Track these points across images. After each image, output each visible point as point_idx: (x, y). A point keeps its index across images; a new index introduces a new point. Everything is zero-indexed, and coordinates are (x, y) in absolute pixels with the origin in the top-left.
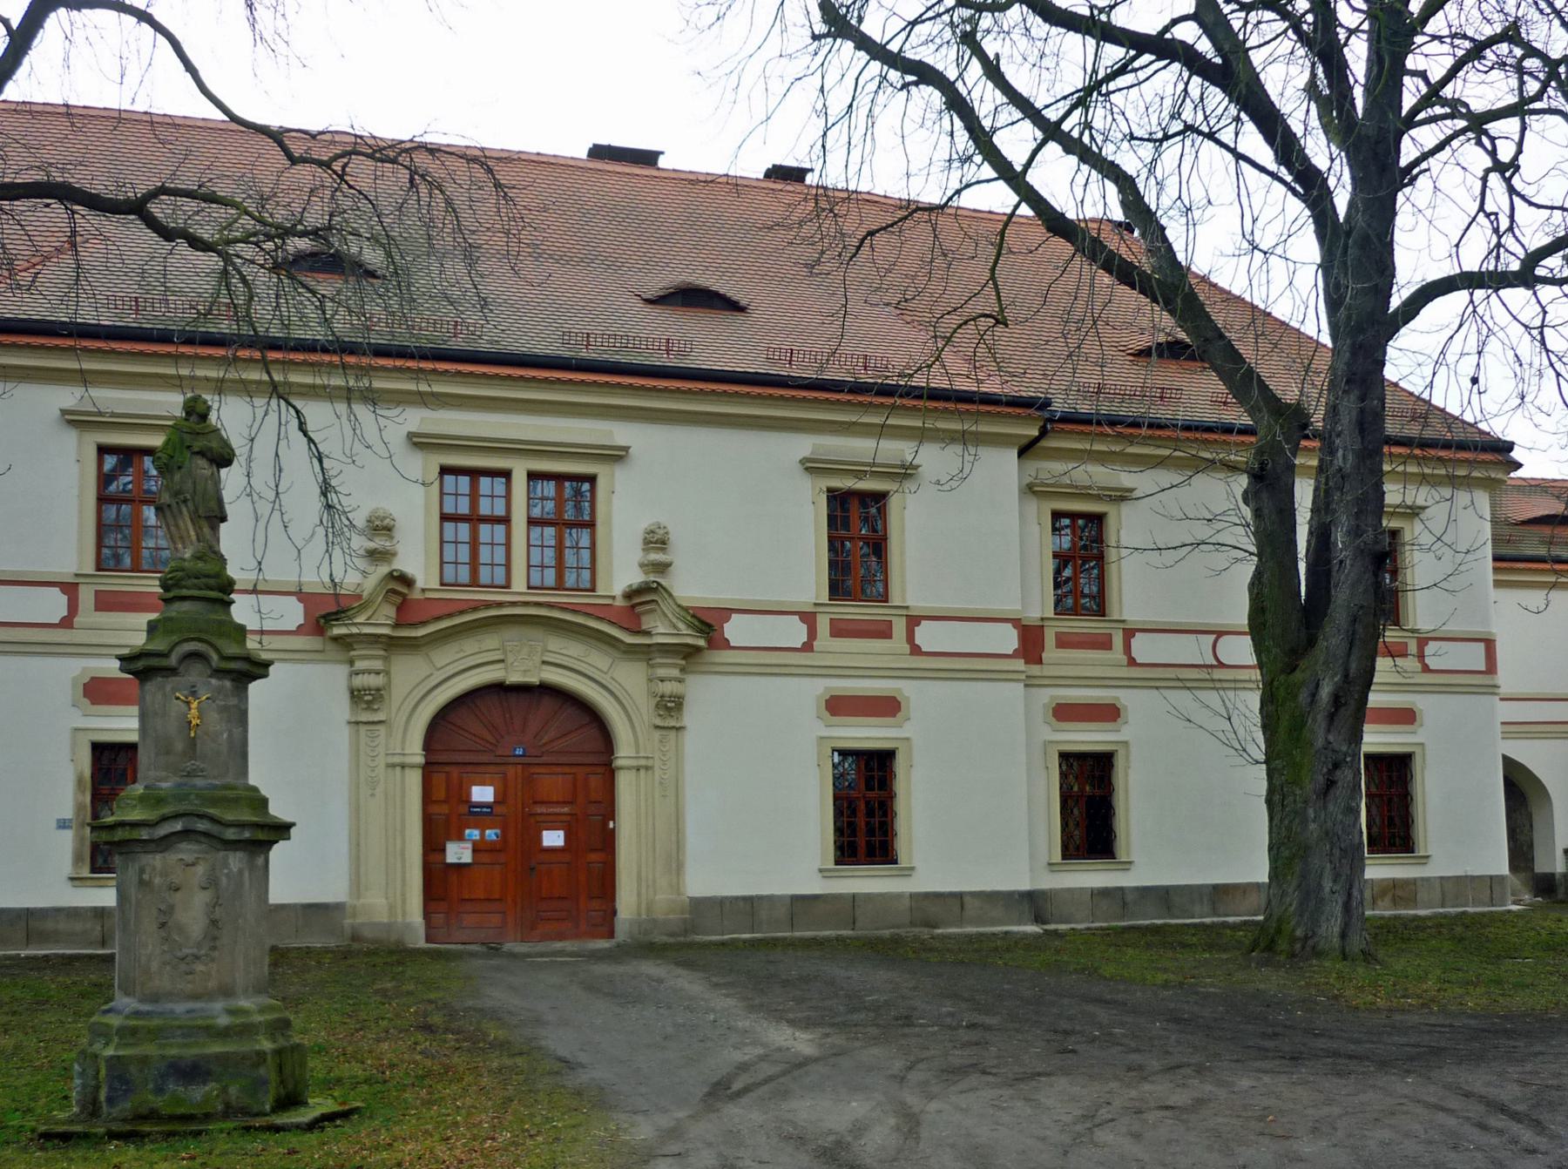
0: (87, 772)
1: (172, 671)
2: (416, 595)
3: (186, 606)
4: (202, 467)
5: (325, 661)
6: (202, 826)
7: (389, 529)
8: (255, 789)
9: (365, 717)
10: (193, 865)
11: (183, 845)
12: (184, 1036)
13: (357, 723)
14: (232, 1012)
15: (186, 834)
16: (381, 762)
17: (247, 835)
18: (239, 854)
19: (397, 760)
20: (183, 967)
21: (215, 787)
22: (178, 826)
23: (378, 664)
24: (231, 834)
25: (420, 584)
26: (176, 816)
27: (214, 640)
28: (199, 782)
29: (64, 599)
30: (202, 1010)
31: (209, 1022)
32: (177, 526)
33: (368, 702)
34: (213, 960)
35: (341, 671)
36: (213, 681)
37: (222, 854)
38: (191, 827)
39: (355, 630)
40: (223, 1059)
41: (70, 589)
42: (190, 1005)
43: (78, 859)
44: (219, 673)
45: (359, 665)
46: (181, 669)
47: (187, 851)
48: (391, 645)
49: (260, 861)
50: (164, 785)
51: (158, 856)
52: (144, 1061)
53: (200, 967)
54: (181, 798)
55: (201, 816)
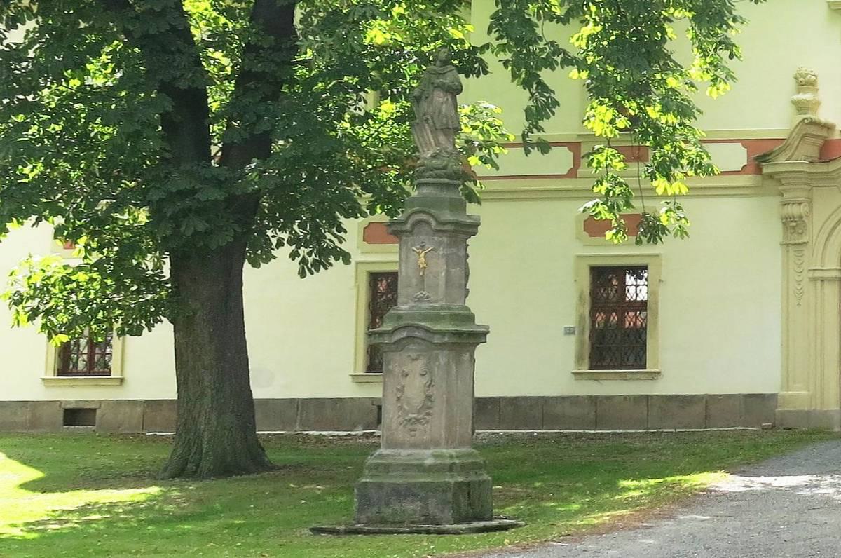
0: (587, 291)
3: (425, 190)
4: (439, 97)
6: (417, 334)
8: (468, 309)
11: (411, 346)
13: (788, 245)
14: (435, 456)
16: (806, 275)
17: (446, 339)
18: (446, 352)
19: (818, 274)
20: (409, 426)
21: (434, 308)
22: (405, 335)
23: (802, 196)
24: (437, 339)
26: (404, 327)
28: (424, 305)
30: (418, 454)
31: (420, 462)
32: (423, 136)
33: (794, 228)
35: (775, 201)
36: (436, 238)
40: (423, 486)
43: (579, 359)
48: (813, 181)
49: (466, 356)
53: (419, 426)
55: (418, 328)
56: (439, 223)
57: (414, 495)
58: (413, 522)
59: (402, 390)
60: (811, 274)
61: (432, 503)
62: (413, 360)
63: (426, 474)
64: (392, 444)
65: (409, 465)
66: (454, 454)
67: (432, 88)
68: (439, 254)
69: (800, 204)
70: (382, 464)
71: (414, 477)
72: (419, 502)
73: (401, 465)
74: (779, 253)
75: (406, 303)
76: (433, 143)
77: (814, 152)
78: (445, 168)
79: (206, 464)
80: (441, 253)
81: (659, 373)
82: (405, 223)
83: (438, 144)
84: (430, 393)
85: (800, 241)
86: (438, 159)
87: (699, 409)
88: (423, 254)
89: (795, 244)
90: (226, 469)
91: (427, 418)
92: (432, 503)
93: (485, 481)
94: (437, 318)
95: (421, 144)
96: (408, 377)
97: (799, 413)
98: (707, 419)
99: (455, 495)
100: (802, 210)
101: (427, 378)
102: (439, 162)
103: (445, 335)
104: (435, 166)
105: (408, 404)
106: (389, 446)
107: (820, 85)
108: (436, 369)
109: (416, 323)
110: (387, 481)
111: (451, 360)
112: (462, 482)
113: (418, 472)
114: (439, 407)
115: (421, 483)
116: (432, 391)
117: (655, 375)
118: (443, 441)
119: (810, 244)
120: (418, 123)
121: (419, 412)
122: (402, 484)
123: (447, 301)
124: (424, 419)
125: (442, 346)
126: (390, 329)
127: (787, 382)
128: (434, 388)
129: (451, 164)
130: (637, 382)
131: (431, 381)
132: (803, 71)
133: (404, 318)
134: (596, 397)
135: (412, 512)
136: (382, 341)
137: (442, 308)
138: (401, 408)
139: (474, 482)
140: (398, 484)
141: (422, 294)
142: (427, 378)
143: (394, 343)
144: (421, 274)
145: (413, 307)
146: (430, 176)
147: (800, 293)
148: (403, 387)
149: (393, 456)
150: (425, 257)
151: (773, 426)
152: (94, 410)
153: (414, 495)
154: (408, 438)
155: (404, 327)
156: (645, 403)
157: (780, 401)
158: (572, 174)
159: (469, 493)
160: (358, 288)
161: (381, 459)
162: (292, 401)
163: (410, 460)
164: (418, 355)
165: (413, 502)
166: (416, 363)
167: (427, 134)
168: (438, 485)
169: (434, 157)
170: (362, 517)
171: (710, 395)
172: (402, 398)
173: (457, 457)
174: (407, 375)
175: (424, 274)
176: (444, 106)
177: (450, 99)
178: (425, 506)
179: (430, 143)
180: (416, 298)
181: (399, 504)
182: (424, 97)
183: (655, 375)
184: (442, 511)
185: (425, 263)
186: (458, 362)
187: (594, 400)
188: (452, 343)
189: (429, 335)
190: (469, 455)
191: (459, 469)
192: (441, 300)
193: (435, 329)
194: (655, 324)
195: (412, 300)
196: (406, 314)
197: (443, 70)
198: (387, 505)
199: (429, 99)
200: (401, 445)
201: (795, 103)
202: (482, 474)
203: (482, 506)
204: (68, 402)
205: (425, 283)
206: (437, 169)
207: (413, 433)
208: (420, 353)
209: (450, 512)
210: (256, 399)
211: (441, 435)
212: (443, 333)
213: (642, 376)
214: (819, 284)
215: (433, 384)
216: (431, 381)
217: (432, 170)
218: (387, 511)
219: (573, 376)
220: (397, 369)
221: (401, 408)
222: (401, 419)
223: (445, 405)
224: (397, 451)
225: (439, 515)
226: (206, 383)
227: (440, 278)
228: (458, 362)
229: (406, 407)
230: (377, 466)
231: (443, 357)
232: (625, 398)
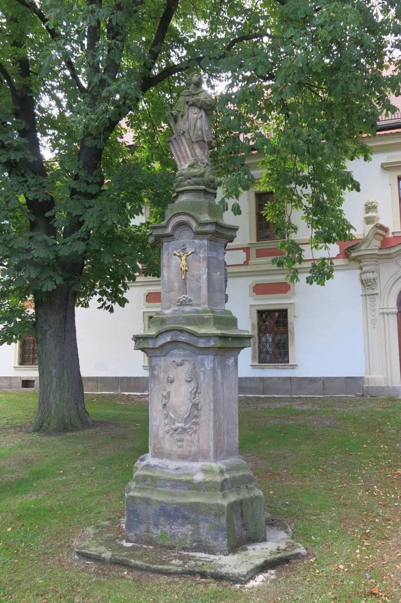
1: (170, 236)
2: (391, 235)
5: (349, 269)
6: (182, 338)
7: (375, 207)
8: (229, 313)
9: (370, 292)
10: (181, 365)
11: (175, 351)
12: (173, 486)
13: (365, 295)
14: (205, 471)
15: (174, 343)
16: (378, 311)
17: (212, 344)
18: (211, 357)
19: (385, 311)
21: (197, 311)
22: (169, 339)
23: (373, 268)
24: (202, 343)
25: (391, 231)
26: (167, 331)
27: (192, 213)
28: (187, 309)
29: (245, 254)
31: (188, 478)
32: (180, 150)
34: (195, 432)
36: (196, 241)
37: (200, 357)
38: (175, 338)
39: (361, 253)
40: (194, 507)
41: (247, 250)
42: (181, 464)
43: (253, 358)
44: (199, 234)
45: (364, 269)
46: (176, 234)
47: (177, 355)
49: (231, 361)
50: (167, 312)
51: (163, 359)
52: (147, 501)
53: (187, 437)
54: (175, 319)
55: (182, 331)
56: (201, 224)
57: (185, 518)
58: (184, 549)
59: (168, 396)
60: (381, 311)
61: (204, 528)
62: (178, 365)
63: (195, 492)
64: (159, 454)
65: (178, 481)
66: (224, 467)
67: (188, 106)
68: (200, 257)
69: (373, 272)
70: (150, 476)
71: (184, 495)
72: (189, 526)
73: (169, 480)
74: (360, 300)
75: (169, 308)
76: (190, 156)
77: (378, 244)
78: (202, 175)
79: (53, 424)
80: (202, 255)
81: (296, 365)
82: (166, 227)
83: (194, 155)
84: (196, 401)
85: (374, 293)
86: (195, 168)
87: (320, 384)
88: (184, 258)
89: (371, 295)
90: (64, 428)
91: (195, 427)
92: (204, 528)
93: (257, 497)
94: (201, 322)
95: (179, 159)
96: (174, 383)
97: (377, 388)
98: (324, 390)
99: (229, 521)
100: (375, 275)
101: (193, 384)
102: (196, 170)
103: (210, 340)
104: (192, 174)
105: (175, 412)
106: (155, 455)
107: (378, 209)
108: (202, 376)
109: (180, 326)
110: (155, 497)
111: (217, 366)
112: (235, 502)
113: (189, 490)
114: (207, 417)
115: (191, 504)
116: (199, 399)
117: (294, 367)
118: (212, 453)
119: (379, 294)
120: (175, 139)
121: (186, 421)
122: (172, 504)
123: (209, 305)
124: (190, 428)
125: (206, 350)
126: (154, 333)
127: (369, 370)
128: (201, 395)
129: (207, 173)
130: (285, 370)
131: (197, 388)
132: (371, 201)
133: (167, 322)
134: (263, 378)
135: (183, 537)
136: (147, 346)
137: (205, 311)
138: (167, 416)
139: (246, 499)
140: (167, 504)
141: (184, 297)
142: (193, 384)
143: (158, 348)
144: (183, 277)
145: (176, 310)
146: (189, 184)
147: (374, 322)
148: (169, 393)
149: (161, 468)
150: (186, 259)
151: (363, 395)
152: (34, 381)
153: (185, 518)
154: (175, 449)
155: (167, 331)
156: (289, 381)
157: (366, 381)
158: (246, 263)
159: (242, 513)
160: (144, 324)
161: (148, 470)
162: (116, 378)
163: (180, 475)
164: (183, 360)
165: (183, 525)
166: (181, 368)
167: (184, 148)
168: (209, 507)
169: (191, 166)
170: (131, 534)
171: (325, 378)
172: (167, 406)
173: (227, 470)
174: (172, 382)
175: (185, 277)
176: (199, 121)
177: (204, 116)
178: (196, 531)
179: (187, 156)
180: (178, 302)
181: (168, 527)
182: (180, 117)
183: (294, 367)
184: (216, 539)
185: (186, 266)
186: (224, 367)
187: (262, 379)
188: (218, 348)
189: (193, 338)
190: (238, 468)
191: (230, 484)
192: (204, 304)
193: (199, 332)
194: (293, 339)
195: (174, 304)
196: (170, 318)
197: (195, 91)
198: (156, 525)
199: (185, 117)
200: (169, 456)
201: (366, 218)
202: (253, 489)
203: (256, 526)
204: (24, 377)
205: (188, 285)
206: (195, 176)
207: (180, 443)
208: (183, 358)
209: (224, 540)
210: (89, 379)
211: (209, 447)
212: (208, 337)
213: (287, 367)
214: (386, 315)
215: (199, 391)
216: (197, 388)
217: (190, 179)
218: (156, 533)
219: (251, 367)
220: (162, 375)
221: (167, 416)
222: (167, 428)
223: (212, 413)
224: (165, 462)
225: (212, 543)
226: (53, 375)
227: (202, 281)
228: (224, 367)
229: (172, 415)
230: (144, 478)
231: (208, 362)
232: (279, 378)
